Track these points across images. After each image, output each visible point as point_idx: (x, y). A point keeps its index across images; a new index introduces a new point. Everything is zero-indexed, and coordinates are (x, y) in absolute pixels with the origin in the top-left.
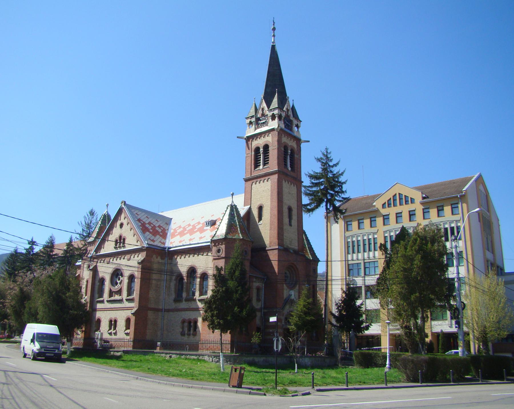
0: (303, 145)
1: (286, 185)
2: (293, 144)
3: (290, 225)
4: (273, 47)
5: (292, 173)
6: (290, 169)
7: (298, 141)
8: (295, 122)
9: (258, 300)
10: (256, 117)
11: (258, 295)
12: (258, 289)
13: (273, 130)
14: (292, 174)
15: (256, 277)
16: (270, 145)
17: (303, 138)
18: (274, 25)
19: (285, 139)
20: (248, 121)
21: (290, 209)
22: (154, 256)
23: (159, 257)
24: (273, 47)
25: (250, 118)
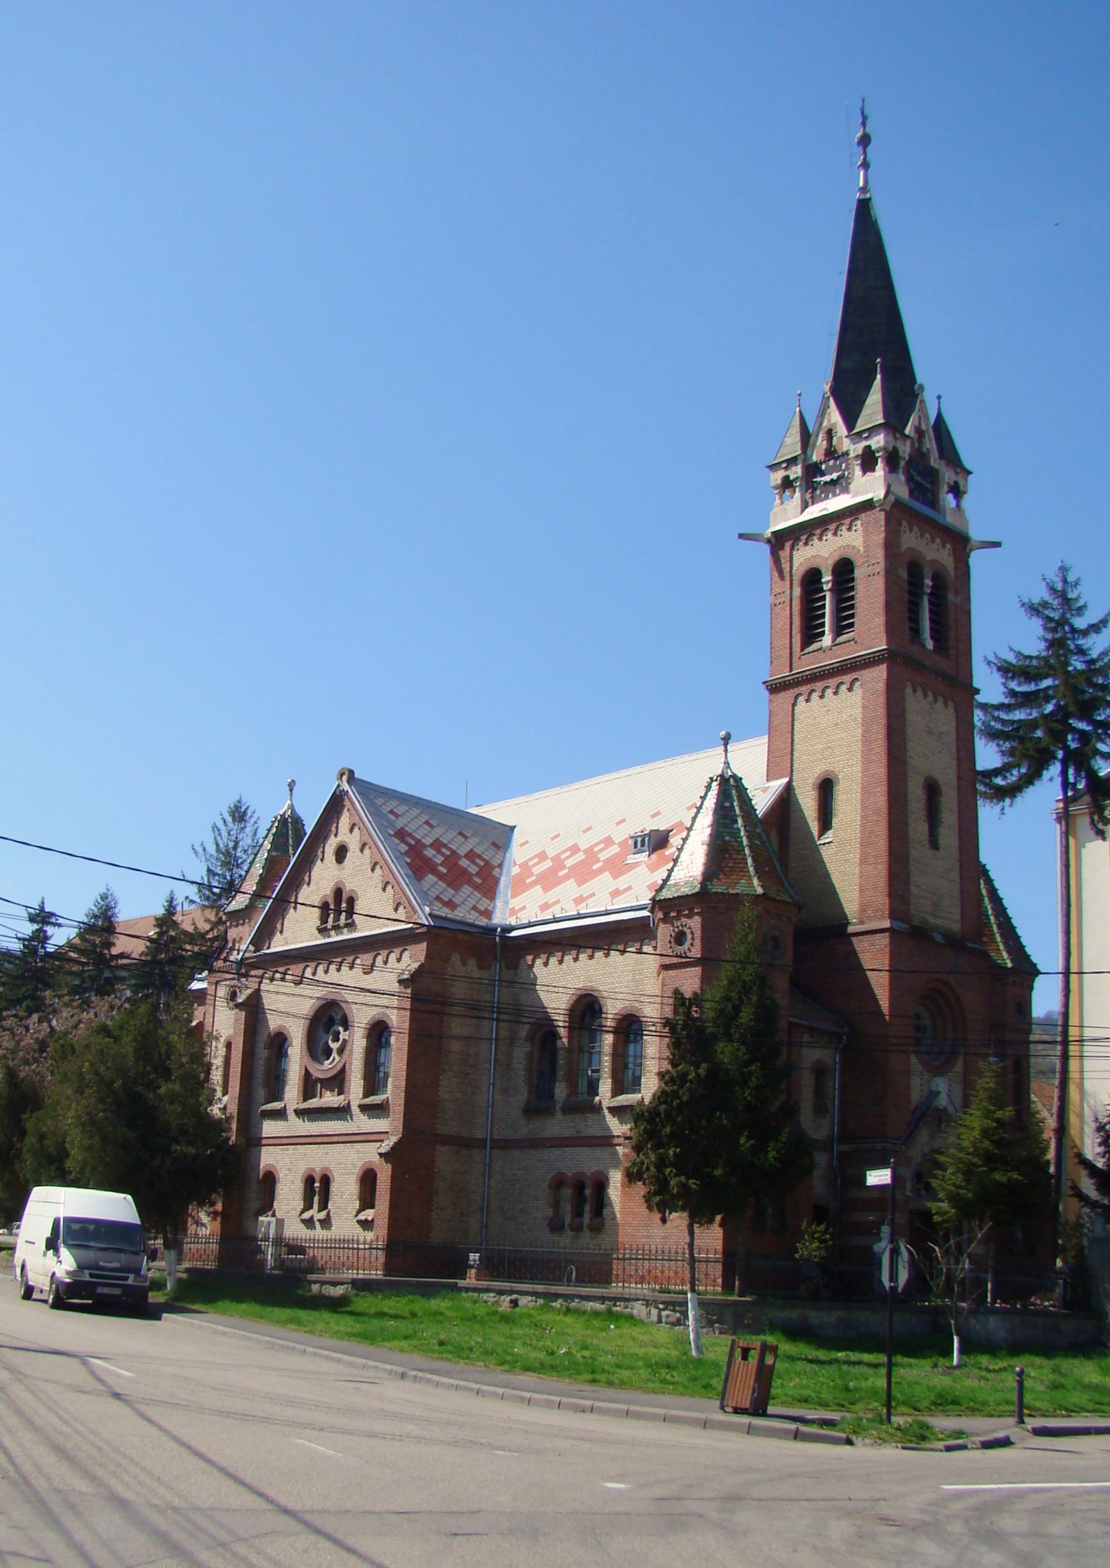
0: (977, 560)
1: (915, 703)
2: (944, 557)
4: (864, 208)
6: (930, 644)
8: (948, 476)
9: (820, 1109)
10: (804, 460)
11: (819, 1091)
12: (820, 1072)
13: (867, 506)
15: (811, 1030)
16: (858, 561)
17: (976, 533)
19: (911, 540)
20: (777, 477)
21: (932, 789)
22: (456, 958)
23: (472, 963)
24: (864, 208)
25: (784, 465)
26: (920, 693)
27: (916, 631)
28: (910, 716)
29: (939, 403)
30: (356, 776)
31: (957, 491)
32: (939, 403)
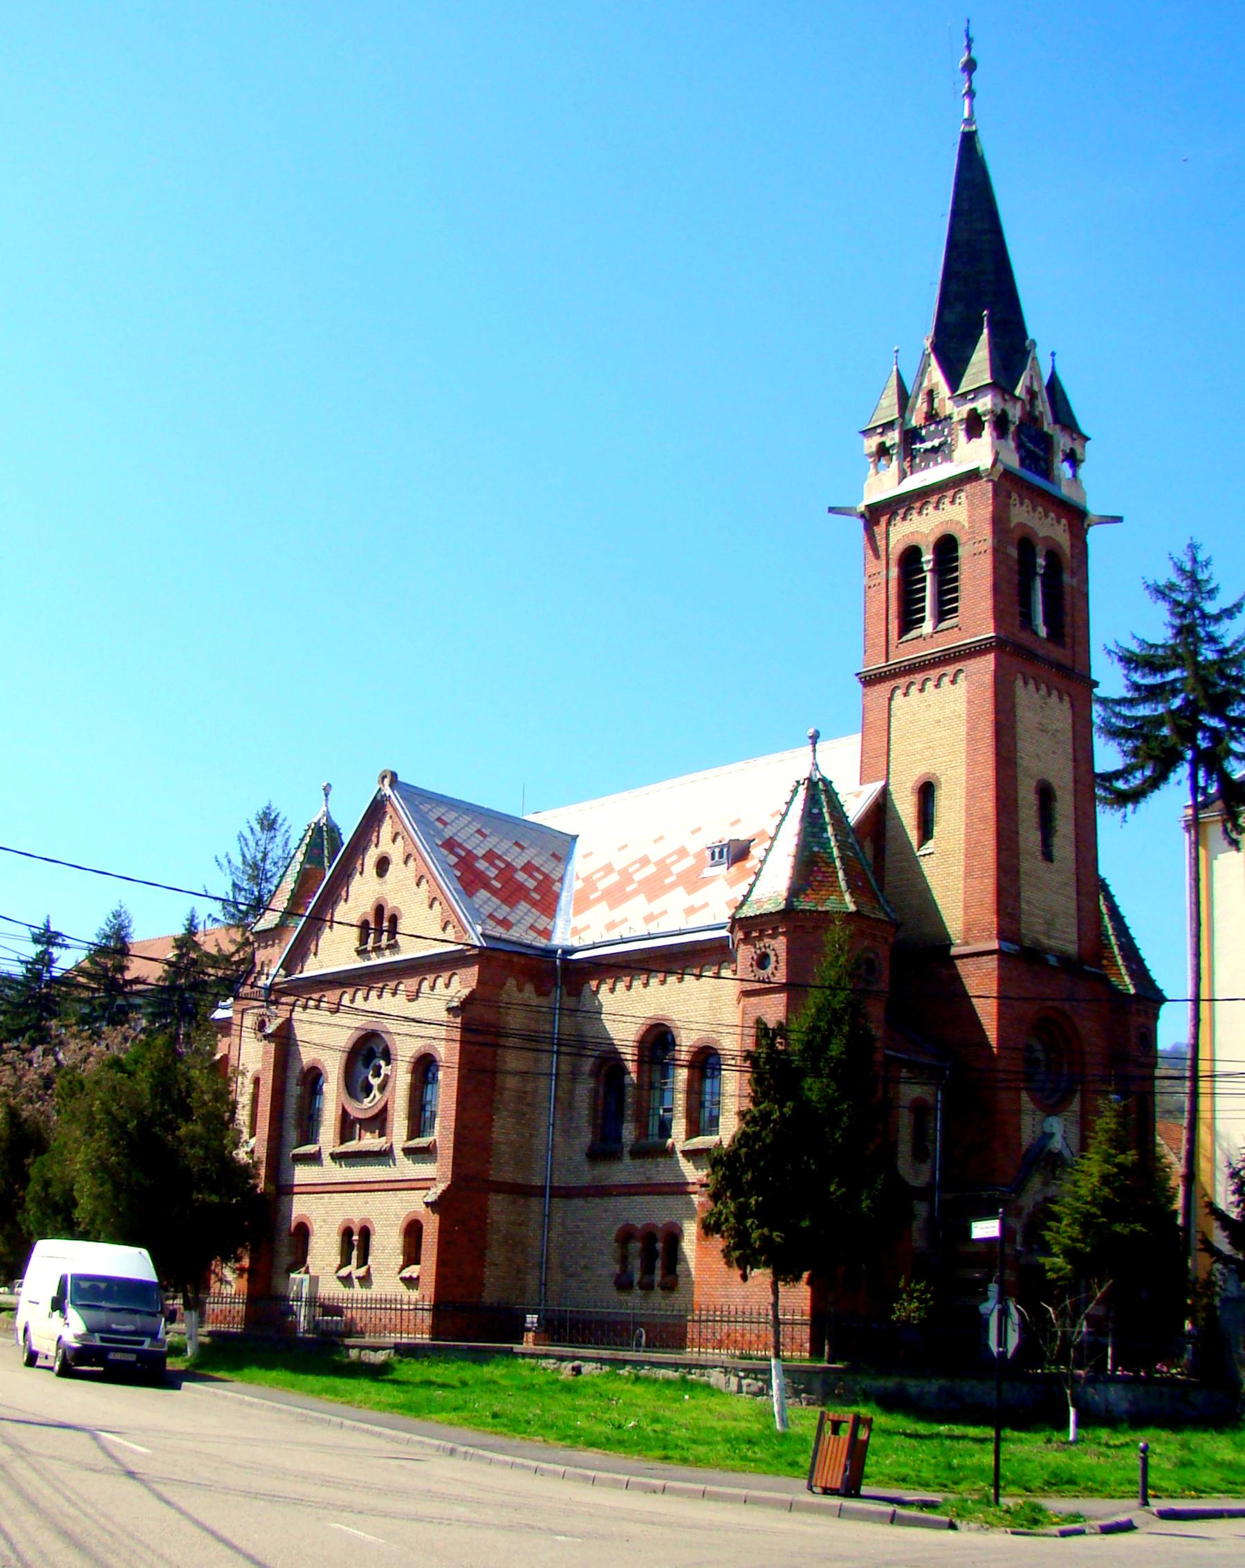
0: (1096, 537)
1: (1026, 696)
3: (1048, 856)
4: (969, 142)
5: (1050, 646)
6: (1043, 631)
7: (1076, 517)
8: (1063, 442)
9: (920, 1153)
10: (902, 425)
12: (920, 1110)
13: (973, 476)
14: (1056, 653)
16: (961, 538)
17: (1094, 507)
18: (969, 48)
19: (1022, 514)
20: (872, 443)
22: (511, 983)
23: (529, 988)
24: (969, 142)
25: (879, 430)
26: (1031, 686)
27: (1026, 620)
28: (1020, 712)
29: (1053, 361)
30: (400, 779)
31: (1073, 460)
32: (1053, 361)
